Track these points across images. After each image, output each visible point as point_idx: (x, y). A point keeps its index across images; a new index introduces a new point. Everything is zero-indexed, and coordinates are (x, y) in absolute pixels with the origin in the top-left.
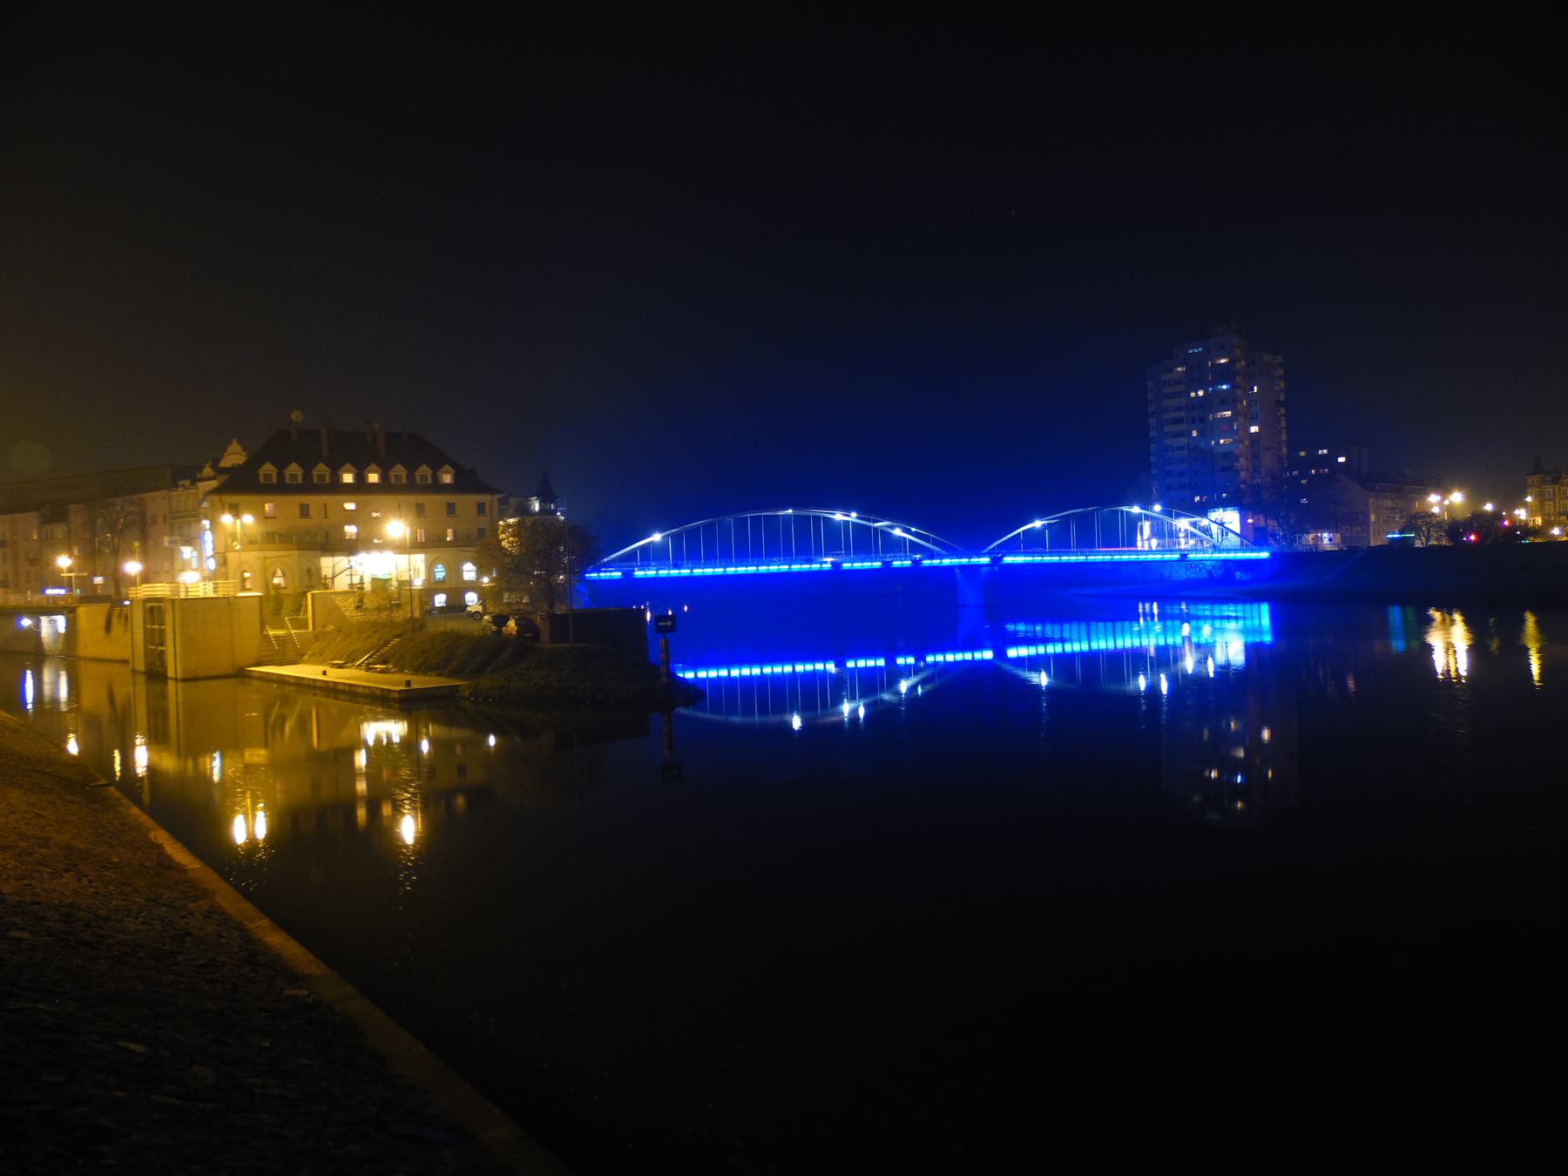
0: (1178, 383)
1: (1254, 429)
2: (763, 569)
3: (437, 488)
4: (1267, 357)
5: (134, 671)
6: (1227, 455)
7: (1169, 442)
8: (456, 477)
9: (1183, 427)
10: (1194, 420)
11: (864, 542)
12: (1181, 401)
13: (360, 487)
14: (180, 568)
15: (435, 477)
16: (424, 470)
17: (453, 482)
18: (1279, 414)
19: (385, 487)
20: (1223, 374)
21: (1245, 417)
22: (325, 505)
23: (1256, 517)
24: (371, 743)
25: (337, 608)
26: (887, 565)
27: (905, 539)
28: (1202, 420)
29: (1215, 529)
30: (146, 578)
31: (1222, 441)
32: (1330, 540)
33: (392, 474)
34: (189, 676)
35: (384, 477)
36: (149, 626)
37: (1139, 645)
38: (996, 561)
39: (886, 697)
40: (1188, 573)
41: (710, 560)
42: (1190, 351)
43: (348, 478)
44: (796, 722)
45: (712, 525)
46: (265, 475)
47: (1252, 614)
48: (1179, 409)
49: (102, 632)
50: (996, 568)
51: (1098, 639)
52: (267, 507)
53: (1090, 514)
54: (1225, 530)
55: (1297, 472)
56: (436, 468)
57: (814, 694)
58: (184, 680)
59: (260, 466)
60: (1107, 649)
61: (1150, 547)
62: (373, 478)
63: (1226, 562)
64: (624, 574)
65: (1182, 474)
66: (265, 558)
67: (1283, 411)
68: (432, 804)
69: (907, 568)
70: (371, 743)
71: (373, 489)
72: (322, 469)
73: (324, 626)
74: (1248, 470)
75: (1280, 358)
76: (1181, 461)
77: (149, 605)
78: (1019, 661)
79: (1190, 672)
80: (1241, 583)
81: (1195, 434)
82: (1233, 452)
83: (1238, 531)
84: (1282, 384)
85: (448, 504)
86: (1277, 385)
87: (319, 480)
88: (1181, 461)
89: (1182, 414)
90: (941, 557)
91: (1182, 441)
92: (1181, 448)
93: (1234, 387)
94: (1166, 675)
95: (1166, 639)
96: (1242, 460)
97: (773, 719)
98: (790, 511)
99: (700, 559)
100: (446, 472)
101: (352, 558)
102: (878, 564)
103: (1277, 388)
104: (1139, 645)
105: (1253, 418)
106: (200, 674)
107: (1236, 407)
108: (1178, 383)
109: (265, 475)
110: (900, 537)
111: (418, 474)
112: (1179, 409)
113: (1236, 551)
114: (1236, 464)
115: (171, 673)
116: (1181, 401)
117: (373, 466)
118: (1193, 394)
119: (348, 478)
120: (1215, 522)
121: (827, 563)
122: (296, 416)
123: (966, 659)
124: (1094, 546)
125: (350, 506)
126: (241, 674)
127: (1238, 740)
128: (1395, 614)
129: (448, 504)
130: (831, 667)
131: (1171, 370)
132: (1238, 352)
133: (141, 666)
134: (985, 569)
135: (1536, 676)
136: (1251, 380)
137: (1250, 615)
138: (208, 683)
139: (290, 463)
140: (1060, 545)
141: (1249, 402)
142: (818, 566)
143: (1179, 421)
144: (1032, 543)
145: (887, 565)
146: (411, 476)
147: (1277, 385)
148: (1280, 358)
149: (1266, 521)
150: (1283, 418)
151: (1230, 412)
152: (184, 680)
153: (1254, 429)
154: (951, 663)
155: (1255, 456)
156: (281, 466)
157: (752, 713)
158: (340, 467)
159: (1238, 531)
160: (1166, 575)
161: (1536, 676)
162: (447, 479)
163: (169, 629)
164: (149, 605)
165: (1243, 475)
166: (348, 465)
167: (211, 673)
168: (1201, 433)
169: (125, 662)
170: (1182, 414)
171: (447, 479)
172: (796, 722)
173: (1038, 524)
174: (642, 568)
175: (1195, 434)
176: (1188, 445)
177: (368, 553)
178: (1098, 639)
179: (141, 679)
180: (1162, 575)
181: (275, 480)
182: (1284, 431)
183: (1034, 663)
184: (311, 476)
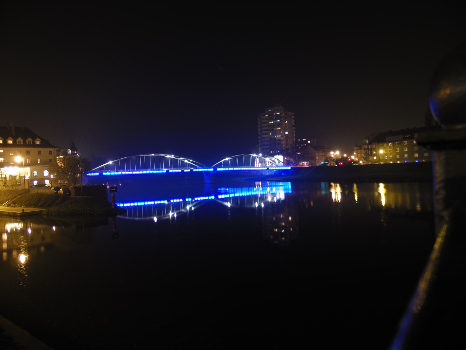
0: (266, 119)
1: (287, 133)
3: (35, 146)
4: (290, 113)
6: (279, 140)
7: (264, 136)
8: (41, 142)
10: (270, 130)
11: (176, 164)
12: (267, 124)
15: (34, 142)
20: (278, 117)
21: (284, 130)
26: (183, 171)
28: (273, 130)
35: (14, 142)
38: (215, 170)
39: (183, 210)
40: (269, 173)
41: (128, 169)
44: (155, 219)
48: (266, 127)
56: (34, 139)
57: (161, 210)
63: (279, 170)
65: (267, 145)
76: (267, 141)
80: (283, 176)
81: (271, 134)
82: (281, 139)
88: (267, 141)
89: (267, 128)
90: (199, 168)
91: (267, 136)
92: (267, 138)
93: (281, 121)
100: (38, 141)
102: (180, 171)
103: (292, 122)
105: (286, 130)
108: (266, 119)
111: (27, 141)
116: (267, 124)
118: (270, 123)
121: (164, 171)
127: (283, 220)
130: (166, 202)
131: (264, 116)
132: (282, 111)
134: (212, 172)
140: (234, 165)
141: (285, 126)
144: (226, 165)
145: (183, 171)
146: (24, 142)
153: (287, 133)
160: (263, 174)
162: (38, 143)
168: (272, 134)
170: (267, 128)
171: (38, 143)
172: (155, 219)
173: (227, 159)
174: (106, 172)
175: (271, 134)
176: (269, 137)
177: (8, 167)
180: (262, 174)
181: (32, 143)
184: (26, 142)
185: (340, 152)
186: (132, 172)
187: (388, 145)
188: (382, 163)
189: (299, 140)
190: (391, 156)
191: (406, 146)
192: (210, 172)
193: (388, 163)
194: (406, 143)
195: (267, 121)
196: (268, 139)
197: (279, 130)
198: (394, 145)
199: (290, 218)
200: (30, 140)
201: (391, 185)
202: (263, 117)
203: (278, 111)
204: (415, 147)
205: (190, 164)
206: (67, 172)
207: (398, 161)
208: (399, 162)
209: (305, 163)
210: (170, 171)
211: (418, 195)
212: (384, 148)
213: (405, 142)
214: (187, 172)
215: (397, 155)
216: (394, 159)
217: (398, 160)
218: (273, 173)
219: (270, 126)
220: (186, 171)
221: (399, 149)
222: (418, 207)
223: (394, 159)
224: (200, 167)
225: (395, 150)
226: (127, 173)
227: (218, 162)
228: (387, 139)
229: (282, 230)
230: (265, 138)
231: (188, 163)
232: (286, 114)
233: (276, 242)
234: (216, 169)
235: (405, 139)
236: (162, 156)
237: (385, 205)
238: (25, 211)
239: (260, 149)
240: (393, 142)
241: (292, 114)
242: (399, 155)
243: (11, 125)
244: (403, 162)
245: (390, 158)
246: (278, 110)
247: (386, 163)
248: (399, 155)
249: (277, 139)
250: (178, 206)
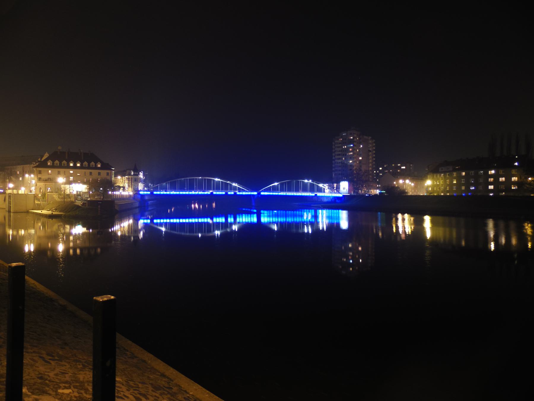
0: (340, 143)
1: (360, 158)
3: (96, 168)
4: (365, 137)
5: (6, 211)
7: (336, 161)
8: (101, 166)
9: (340, 157)
11: (226, 187)
12: (340, 149)
13: (75, 167)
14: (32, 186)
15: (96, 165)
16: (93, 164)
17: (100, 167)
19: (81, 167)
20: (351, 142)
21: (358, 155)
24: (74, 234)
25: (54, 198)
26: (226, 193)
28: (346, 155)
30: (13, 189)
33: (84, 164)
34: (15, 212)
35: (81, 165)
38: (259, 194)
41: (175, 190)
42: (343, 134)
43: (71, 165)
44: (200, 235)
45: (291, 181)
46: (92, 165)
48: (340, 151)
49: (3, 201)
50: (260, 196)
51: (231, 217)
52: (50, 171)
53: (291, 181)
58: (14, 212)
59: (91, 162)
62: (78, 165)
64: (226, 193)
65: (340, 170)
66: (46, 185)
68: (81, 250)
69: (224, 195)
70: (74, 234)
71: (78, 168)
72: (64, 162)
73: (50, 202)
76: (340, 167)
77: (9, 195)
78: (157, 224)
79: (321, 229)
80: (337, 203)
81: (344, 159)
85: (90, 172)
87: (64, 165)
90: (244, 191)
91: (340, 161)
92: (340, 163)
93: (353, 145)
95: (286, 219)
96: (355, 167)
97: (195, 234)
98: (201, 178)
99: (286, 191)
100: (99, 164)
101: (70, 185)
102: (224, 193)
104: (242, 221)
105: (360, 155)
106: (18, 211)
108: (340, 143)
109: (92, 165)
112: (340, 151)
114: (353, 168)
115: (12, 211)
116: (340, 149)
117: (79, 162)
118: (344, 147)
119: (71, 165)
121: (209, 193)
122: (60, 148)
123: (184, 222)
124: (291, 191)
125: (71, 172)
126: (28, 212)
128: (400, 216)
129: (90, 172)
132: (355, 135)
133: (7, 210)
134: (256, 196)
135: (11, 240)
136: (360, 143)
139: (63, 161)
140: (282, 190)
143: (339, 155)
144: (275, 189)
146: (89, 165)
151: (352, 153)
152: (14, 212)
153: (360, 158)
154: (181, 223)
156: (53, 161)
157: (187, 233)
158: (70, 161)
160: (322, 200)
161: (11, 240)
162: (99, 166)
163: (11, 200)
164: (9, 195)
166: (99, 162)
167: (22, 211)
168: (345, 159)
169: (5, 209)
172: (200, 235)
173: (276, 184)
176: (342, 162)
178: (231, 217)
179: (7, 212)
180: (321, 200)
181: (94, 166)
183: (161, 224)
185: (400, 179)
186: (179, 192)
187: (440, 176)
188: (435, 194)
189: (393, 165)
190: (442, 188)
191: (455, 178)
192: (254, 195)
193: (440, 195)
194: (455, 174)
195: (340, 145)
196: (340, 164)
197: (351, 155)
198: (445, 176)
199: (360, 249)
200: (93, 164)
201: (440, 219)
202: (336, 141)
203: (351, 135)
204: (462, 180)
205: (238, 187)
206: (63, 191)
207: (448, 193)
208: (448, 194)
209: (128, 192)
210: (215, 193)
211: (463, 231)
212: (433, 179)
213: (454, 173)
214: (231, 195)
215: (447, 187)
216: (445, 191)
217: (448, 192)
218: (330, 200)
219: (343, 151)
220: (229, 193)
221: (449, 180)
222: (463, 243)
223: (444, 191)
224: (248, 191)
225: (445, 181)
226: (175, 193)
227: (265, 187)
228: (440, 170)
229: (361, 262)
230: (337, 163)
231: (237, 187)
232: (360, 139)
233: (344, 272)
234: (153, 192)
235: (454, 170)
236: (212, 179)
237: (430, 238)
238: (53, 214)
239: (334, 175)
240: (445, 172)
241: (369, 139)
242: (449, 187)
243: (82, 151)
244: (452, 194)
245: (442, 190)
246: (351, 134)
247: (438, 195)
248: (449, 187)
249: (349, 164)
250: (226, 225)
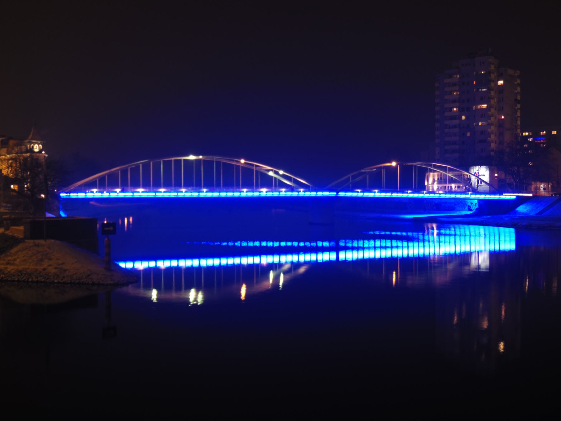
2: (223, 194)
18: (516, 108)
22: (484, 175)
23: (499, 172)
27: (275, 178)
29: (473, 179)
31: (480, 123)
32: (544, 189)
36: (351, 189)
37: (469, 251)
47: (424, 237)
54: (480, 181)
55: (527, 145)
60: (375, 258)
61: (433, 189)
67: (519, 106)
74: (496, 143)
75: (518, 72)
83: (488, 182)
84: (519, 89)
86: (516, 90)
92: (455, 126)
94: (269, 282)
96: (493, 136)
107: (490, 102)
110: (272, 177)
113: (485, 193)
114: (488, 138)
120: (474, 175)
132: (492, 67)
137: (444, 240)
138: (484, 241)
142: (278, 193)
147: (516, 90)
148: (518, 72)
149: (506, 176)
150: (519, 111)
155: (501, 134)
159: (488, 182)
165: (493, 145)
182: (519, 119)
